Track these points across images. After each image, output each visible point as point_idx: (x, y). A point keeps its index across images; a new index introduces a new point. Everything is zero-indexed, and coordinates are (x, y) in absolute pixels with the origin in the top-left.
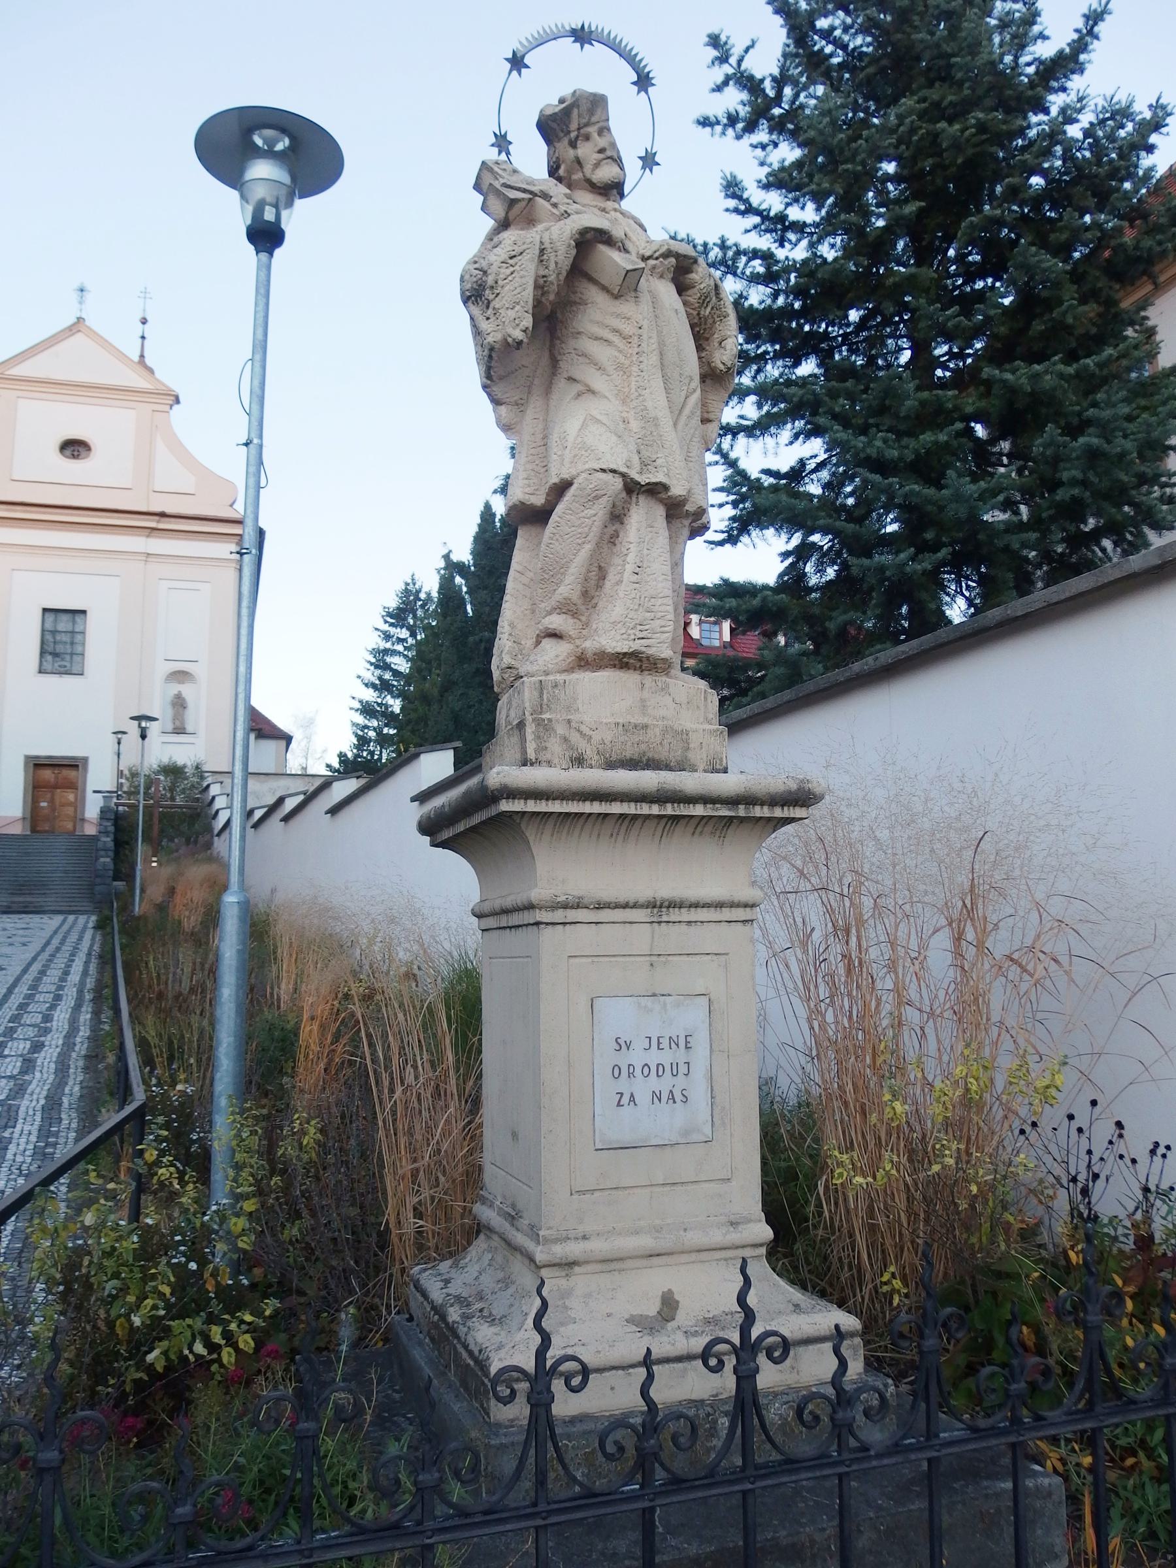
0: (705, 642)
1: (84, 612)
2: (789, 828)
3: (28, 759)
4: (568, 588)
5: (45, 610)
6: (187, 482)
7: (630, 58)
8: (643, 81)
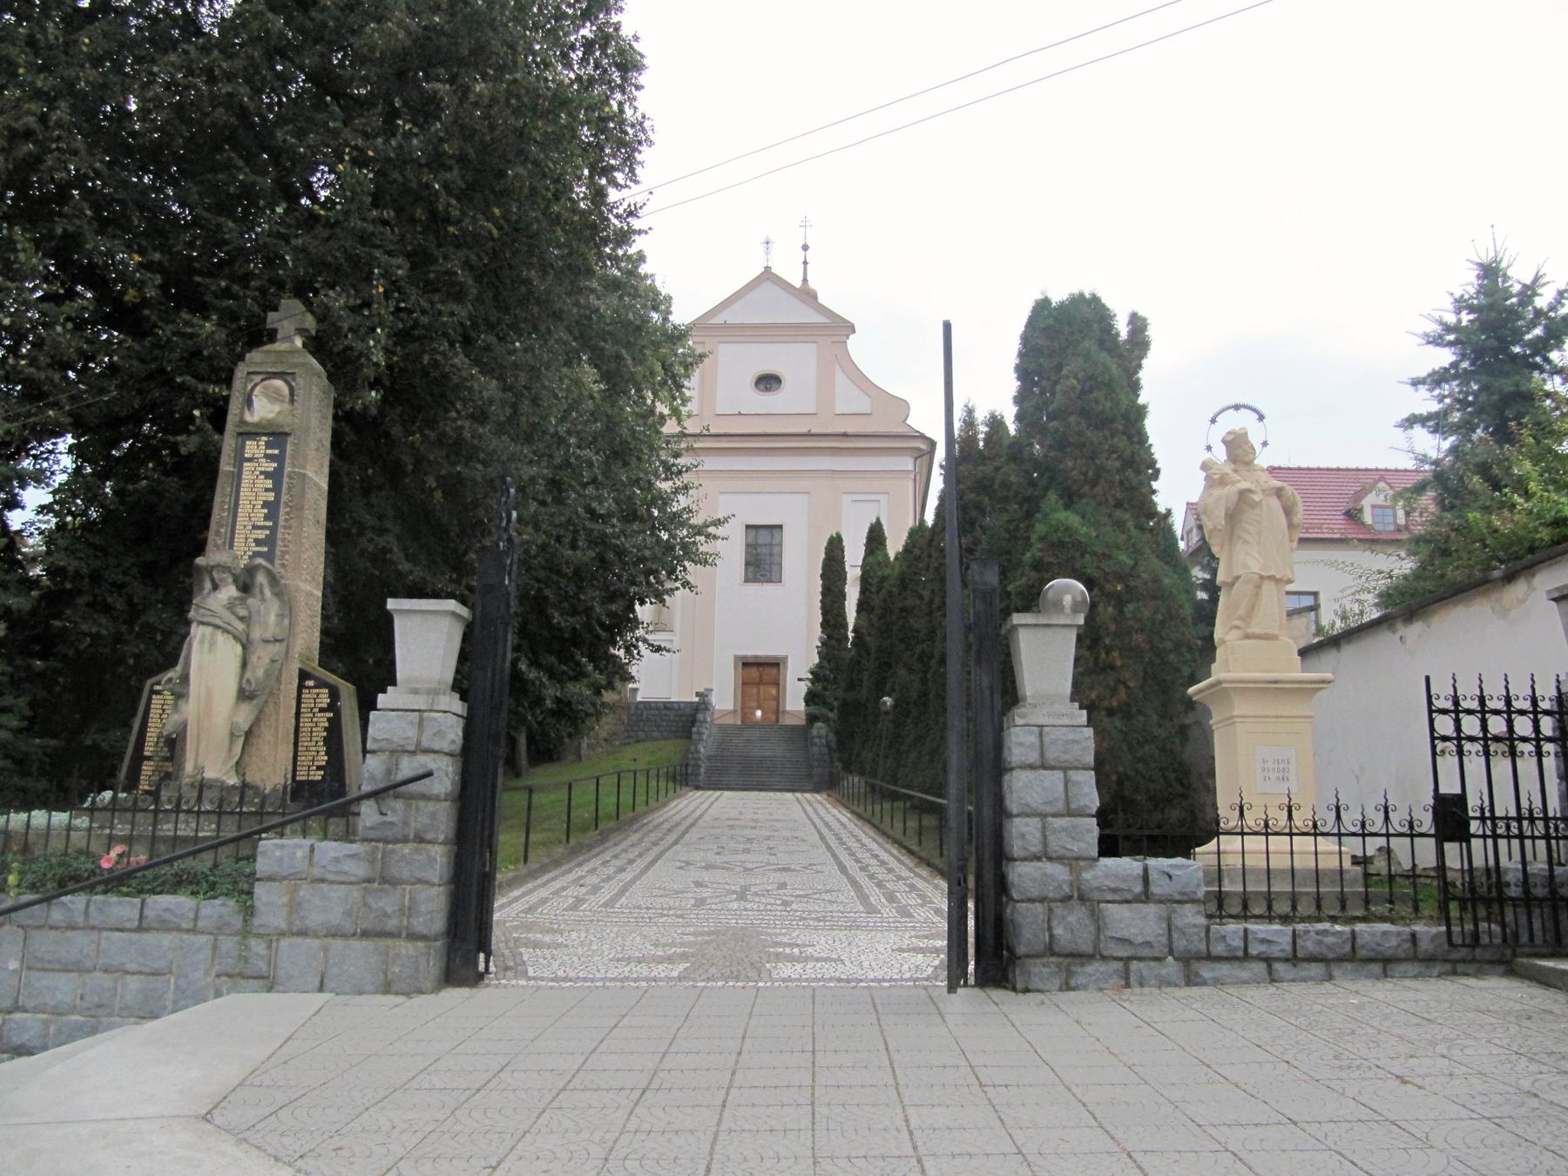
0: (1379, 527)
1: (780, 527)
2: (1320, 693)
3: (737, 658)
4: (1242, 611)
5: (748, 527)
6: (863, 405)
7: (1254, 410)
8: (1261, 418)
